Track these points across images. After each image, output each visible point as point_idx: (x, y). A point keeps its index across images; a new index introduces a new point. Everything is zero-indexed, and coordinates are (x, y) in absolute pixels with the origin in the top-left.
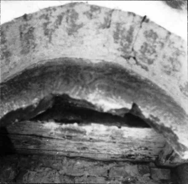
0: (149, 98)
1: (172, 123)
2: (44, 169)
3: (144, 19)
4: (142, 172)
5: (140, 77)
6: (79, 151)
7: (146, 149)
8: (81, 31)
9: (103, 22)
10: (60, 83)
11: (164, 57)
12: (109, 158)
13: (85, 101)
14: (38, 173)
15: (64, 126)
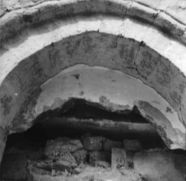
12: (160, 92)
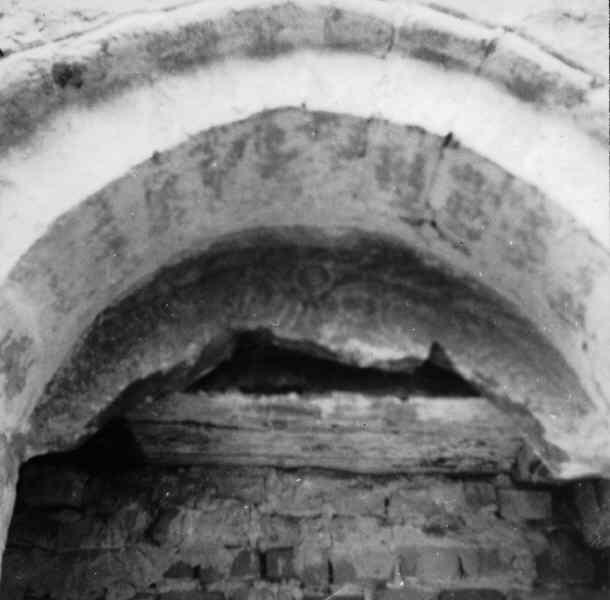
0: (471, 327)
1: (532, 391)
2: (222, 503)
3: (449, 141)
4: (475, 502)
5: (451, 270)
6: (307, 455)
7: (481, 444)
8: (294, 167)
9: (345, 142)
10: (247, 299)
11: (505, 226)
12: (387, 467)
13: (312, 344)
14: (206, 513)
15: (264, 400)
